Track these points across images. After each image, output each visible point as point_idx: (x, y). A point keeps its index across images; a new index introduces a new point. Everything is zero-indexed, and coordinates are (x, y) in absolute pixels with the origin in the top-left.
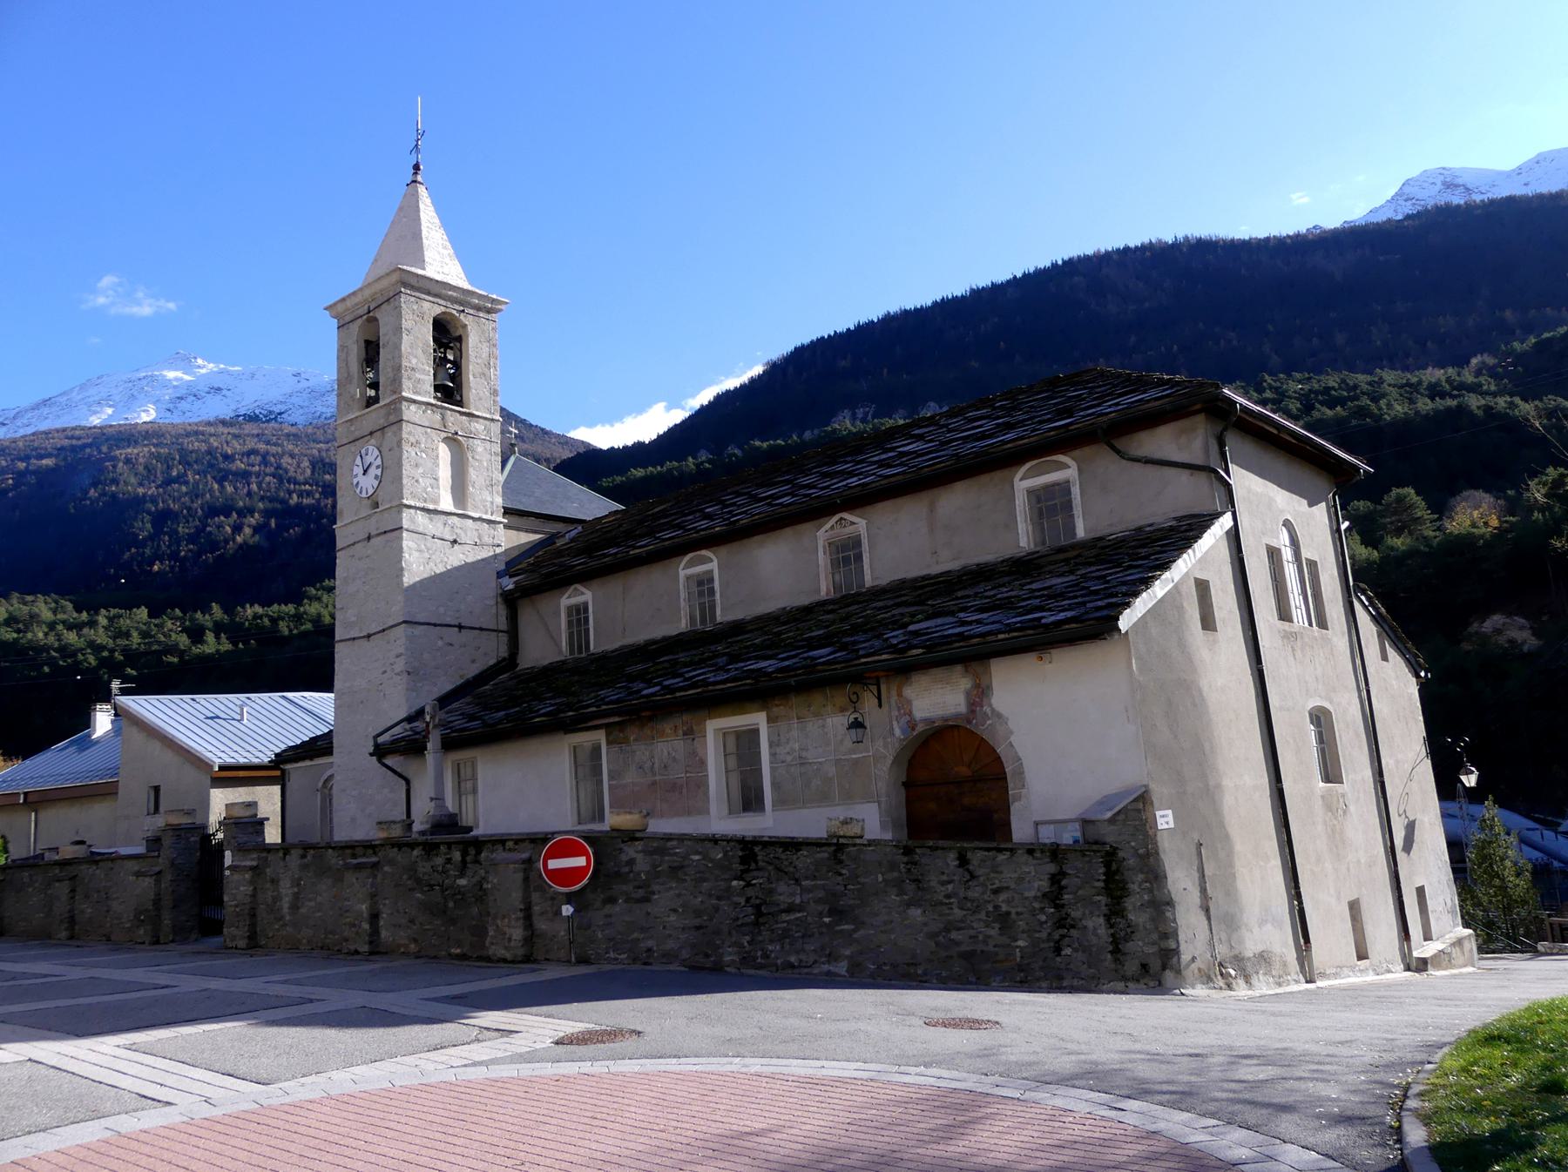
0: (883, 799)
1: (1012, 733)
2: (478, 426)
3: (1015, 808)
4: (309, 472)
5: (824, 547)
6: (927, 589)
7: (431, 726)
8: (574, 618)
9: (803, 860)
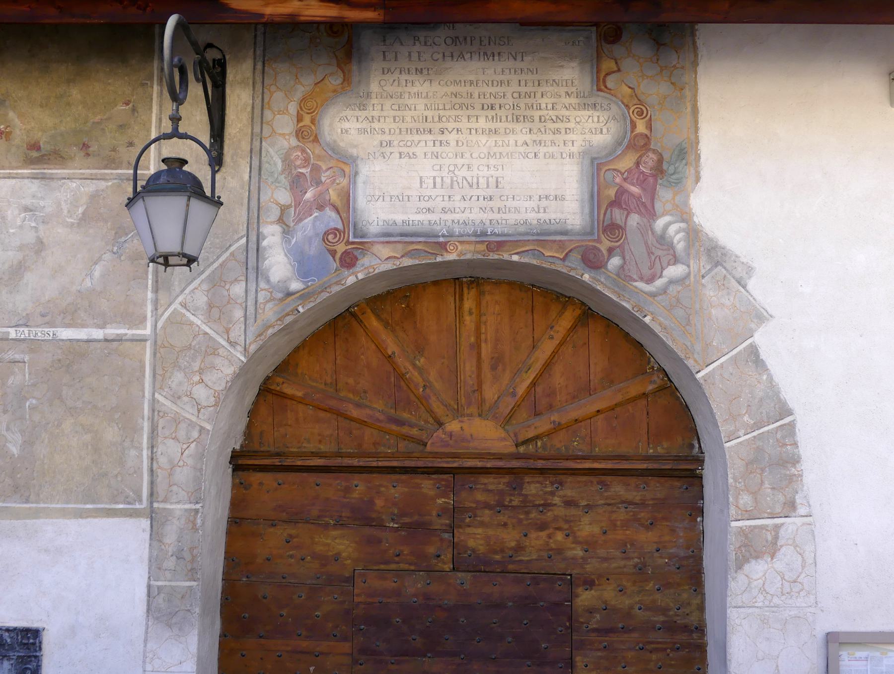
0: (178, 507)
1: (760, 317)
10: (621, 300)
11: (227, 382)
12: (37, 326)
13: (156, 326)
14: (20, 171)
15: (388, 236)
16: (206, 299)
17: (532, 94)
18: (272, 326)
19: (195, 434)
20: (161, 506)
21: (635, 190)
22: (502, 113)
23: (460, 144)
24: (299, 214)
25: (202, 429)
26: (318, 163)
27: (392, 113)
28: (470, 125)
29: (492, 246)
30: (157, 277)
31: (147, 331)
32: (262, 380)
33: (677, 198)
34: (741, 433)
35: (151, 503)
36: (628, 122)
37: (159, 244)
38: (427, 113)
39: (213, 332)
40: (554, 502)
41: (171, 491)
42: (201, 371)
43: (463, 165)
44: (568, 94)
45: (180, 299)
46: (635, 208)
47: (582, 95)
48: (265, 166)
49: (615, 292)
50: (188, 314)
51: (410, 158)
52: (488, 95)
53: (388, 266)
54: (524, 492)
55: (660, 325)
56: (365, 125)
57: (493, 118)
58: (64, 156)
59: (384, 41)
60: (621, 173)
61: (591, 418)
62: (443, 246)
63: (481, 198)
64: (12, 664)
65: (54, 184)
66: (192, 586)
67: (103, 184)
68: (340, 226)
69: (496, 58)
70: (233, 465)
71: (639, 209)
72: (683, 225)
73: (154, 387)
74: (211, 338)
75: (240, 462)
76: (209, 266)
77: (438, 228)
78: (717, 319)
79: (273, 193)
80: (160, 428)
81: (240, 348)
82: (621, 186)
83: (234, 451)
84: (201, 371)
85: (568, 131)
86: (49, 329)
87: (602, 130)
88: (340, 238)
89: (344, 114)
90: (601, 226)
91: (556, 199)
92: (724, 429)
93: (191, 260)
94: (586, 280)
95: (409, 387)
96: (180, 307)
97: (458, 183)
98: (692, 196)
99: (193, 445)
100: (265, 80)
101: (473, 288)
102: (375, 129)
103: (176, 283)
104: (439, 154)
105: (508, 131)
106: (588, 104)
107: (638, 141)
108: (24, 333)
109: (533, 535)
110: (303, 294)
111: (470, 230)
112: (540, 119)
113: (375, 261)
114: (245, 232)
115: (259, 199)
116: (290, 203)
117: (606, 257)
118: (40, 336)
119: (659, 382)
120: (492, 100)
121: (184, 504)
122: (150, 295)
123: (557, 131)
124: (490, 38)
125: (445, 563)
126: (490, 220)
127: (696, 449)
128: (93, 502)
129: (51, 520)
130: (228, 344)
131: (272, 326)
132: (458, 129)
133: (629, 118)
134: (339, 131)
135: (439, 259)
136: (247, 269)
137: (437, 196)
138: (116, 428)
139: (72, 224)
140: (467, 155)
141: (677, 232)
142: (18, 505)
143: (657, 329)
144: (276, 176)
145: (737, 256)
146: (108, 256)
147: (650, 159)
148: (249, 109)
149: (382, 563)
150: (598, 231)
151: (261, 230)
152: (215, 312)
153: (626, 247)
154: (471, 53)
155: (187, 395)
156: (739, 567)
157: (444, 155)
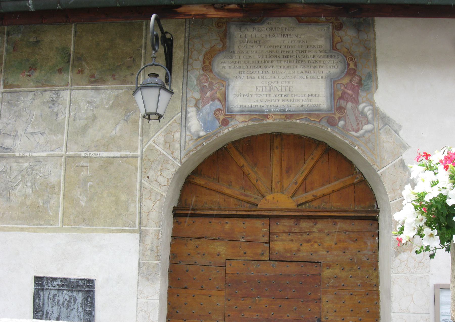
0: (152, 229)
10: (344, 139)
11: (172, 175)
12: (93, 151)
13: (142, 151)
14: (86, 87)
15: (242, 112)
16: (163, 139)
17: (305, 51)
18: (192, 151)
19: (159, 198)
20: (144, 228)
21: (350, 92)
22: (291, 59)
23: (274, 72)
24: (204, 103)
25: (162, 195)
26: (212, 81)
27: (244, 60)
28: (278, 65)
29: (288, 116)
30: (143, 130)
31: (139, 153)
32: (186, 177)
33: (368, 96)
34: (397, 198)
35: (140, 227)
36: (346, 64)
37: (147, 109)
38: (259, 59)
39: (166, 153)
40: (314, 231)
41: (148, 222)
42: (161, 170)
43: (275, 81)
44: (320, 52)
45: (152, 139)
46: (350, 100)
47: (326, 52)
48: (189, 82)
49: (342, 136)
50: (156, 146)
51: (252, 78)
52: (285, 52)
53: (242, 125)
54: (300, 226)
55: (362, 150)
56: (232, 65)
57: (288, 61)
58: (105, 80)
59: (240, 29)
60: (344, 85)
61: (330, 194)
62: (266, 117)
63: (283, 96)
64: (83, 294)
65: (101, 91)
66: (157, 263)
67: (120, 91)
68: (221, 108)
69: (289, 36)
70: (174, 213)
71: (352, 100)
72: (371, 107)
73: (141, 177)
74: (166, 156)
75: (177, 212)
76: (165, 125)
77: (264, 109)
78: (386, 148)
79: (192, 94)
80: (144, 195)
81: (178, 160)
82: (344, 91)
83: (174, 207)
84: (161, 170)
85: (320, 67)
86: (97, 153)
87: (335, 67)
88: (221, 113)
89: (223, 60)
90: (335, 107)
91: (316, 96)
92: (390, 196)
93: (160, 117)
94: (329, 131)
95: (250, 180)
96: (152, 143)
97: (273, 89)
98: (375, 95)
99: (158, 202)
100: (189, 46)
101: (278, 137)
102: (236, 66)
103: (151, 133)
104: (265, 77)
105: (294, 67)
106: (329, 56)
107: (351, 72)
108: (87, 154)
109: (305, 244)
110: (205, 137)
111: (278, 109)
112: (308, 62)
113: (237, 123)
114: (180, 111)
115: (186, 96)
116: (199, 98)
117: (338, 121)
118: (94, 156)
119: (359, 178)
120: (287, 54)
121: (154, 228)
122: (140, 138)
123: (316, 67)
124: (286, 28)
125: (266, 257)
126: (287, 105)
127: (376, 208)
128: (116, 226)
129: (98, 234)
130: (173, 159)
131: (192, 151)
132: (272, 66)
133: (347, 62)
134: (221, 67)
135: (265, 122)
136: (181, 126)
137: (264, 95)
138: (125, 195)
139: (108, 108)
140: (277, 77)
141: (369, 110)
142: (85, 227)
143: (360, 152)
144: (194, 86)
145: (394, 121)
146: (122, 122)
147: (356, 79)
148: (182, 59)
149: (238, 257)
150: (334, 110)
151: (187, 110)
152: (167, 145)
153: (346, 117)
154: (278, 34)
155: (155, 181)
156: (396, 255)
157: (267, 77)
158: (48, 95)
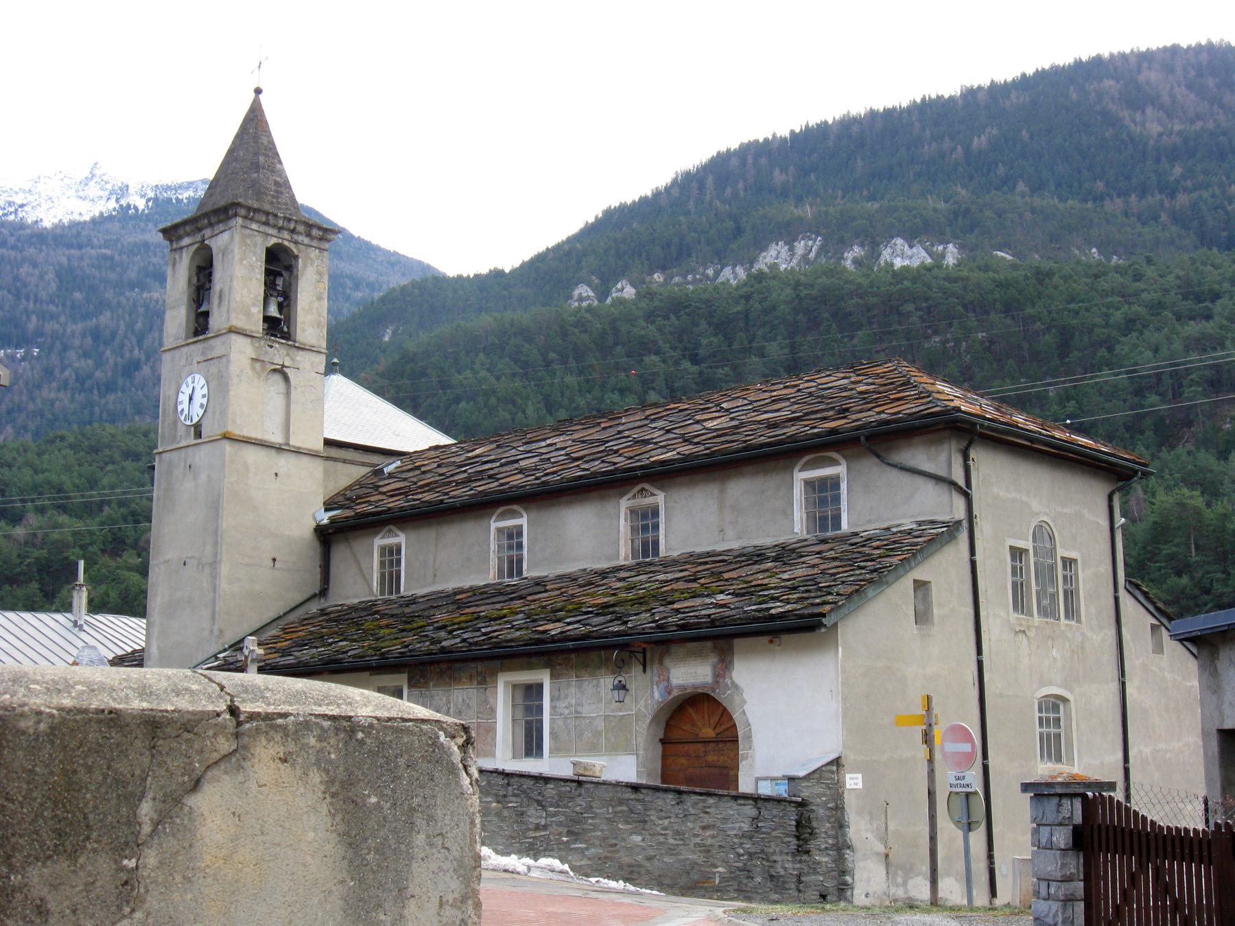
0: (641, 752)
2: (301, 357)
3: (743, 766)
4: (54, 286)
5: (626, 514)
6: (708, 566)
7: (249, 659)
8: (387, 570)
9: (550, 790)
158: (595, 681)
